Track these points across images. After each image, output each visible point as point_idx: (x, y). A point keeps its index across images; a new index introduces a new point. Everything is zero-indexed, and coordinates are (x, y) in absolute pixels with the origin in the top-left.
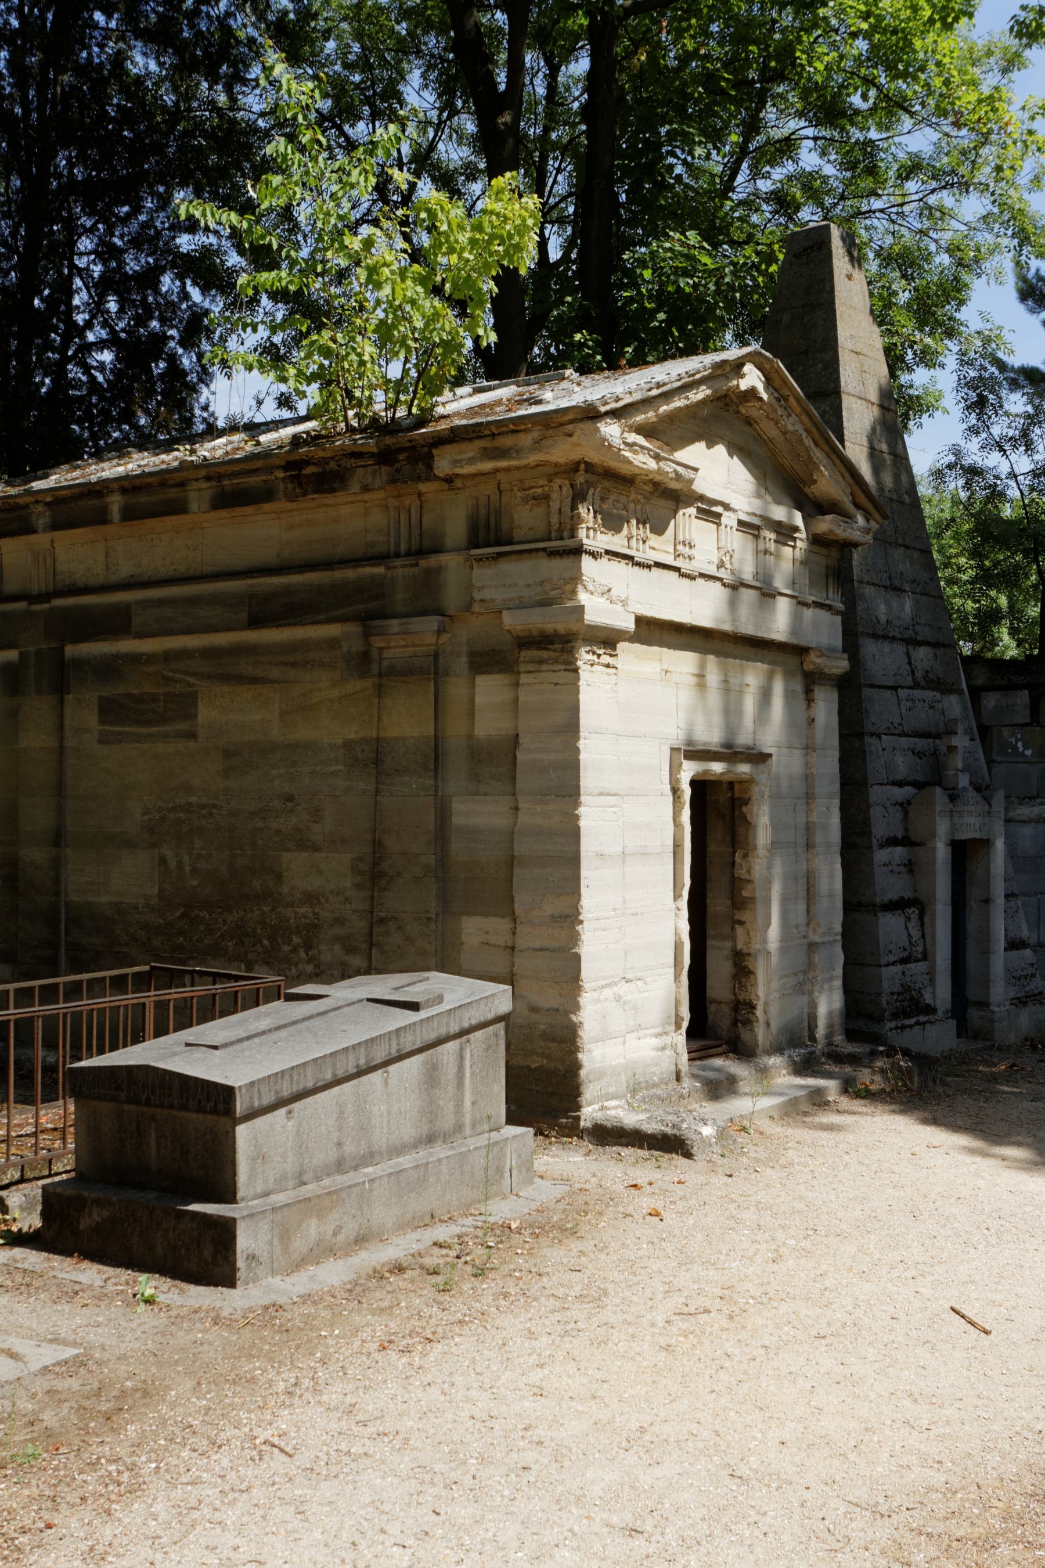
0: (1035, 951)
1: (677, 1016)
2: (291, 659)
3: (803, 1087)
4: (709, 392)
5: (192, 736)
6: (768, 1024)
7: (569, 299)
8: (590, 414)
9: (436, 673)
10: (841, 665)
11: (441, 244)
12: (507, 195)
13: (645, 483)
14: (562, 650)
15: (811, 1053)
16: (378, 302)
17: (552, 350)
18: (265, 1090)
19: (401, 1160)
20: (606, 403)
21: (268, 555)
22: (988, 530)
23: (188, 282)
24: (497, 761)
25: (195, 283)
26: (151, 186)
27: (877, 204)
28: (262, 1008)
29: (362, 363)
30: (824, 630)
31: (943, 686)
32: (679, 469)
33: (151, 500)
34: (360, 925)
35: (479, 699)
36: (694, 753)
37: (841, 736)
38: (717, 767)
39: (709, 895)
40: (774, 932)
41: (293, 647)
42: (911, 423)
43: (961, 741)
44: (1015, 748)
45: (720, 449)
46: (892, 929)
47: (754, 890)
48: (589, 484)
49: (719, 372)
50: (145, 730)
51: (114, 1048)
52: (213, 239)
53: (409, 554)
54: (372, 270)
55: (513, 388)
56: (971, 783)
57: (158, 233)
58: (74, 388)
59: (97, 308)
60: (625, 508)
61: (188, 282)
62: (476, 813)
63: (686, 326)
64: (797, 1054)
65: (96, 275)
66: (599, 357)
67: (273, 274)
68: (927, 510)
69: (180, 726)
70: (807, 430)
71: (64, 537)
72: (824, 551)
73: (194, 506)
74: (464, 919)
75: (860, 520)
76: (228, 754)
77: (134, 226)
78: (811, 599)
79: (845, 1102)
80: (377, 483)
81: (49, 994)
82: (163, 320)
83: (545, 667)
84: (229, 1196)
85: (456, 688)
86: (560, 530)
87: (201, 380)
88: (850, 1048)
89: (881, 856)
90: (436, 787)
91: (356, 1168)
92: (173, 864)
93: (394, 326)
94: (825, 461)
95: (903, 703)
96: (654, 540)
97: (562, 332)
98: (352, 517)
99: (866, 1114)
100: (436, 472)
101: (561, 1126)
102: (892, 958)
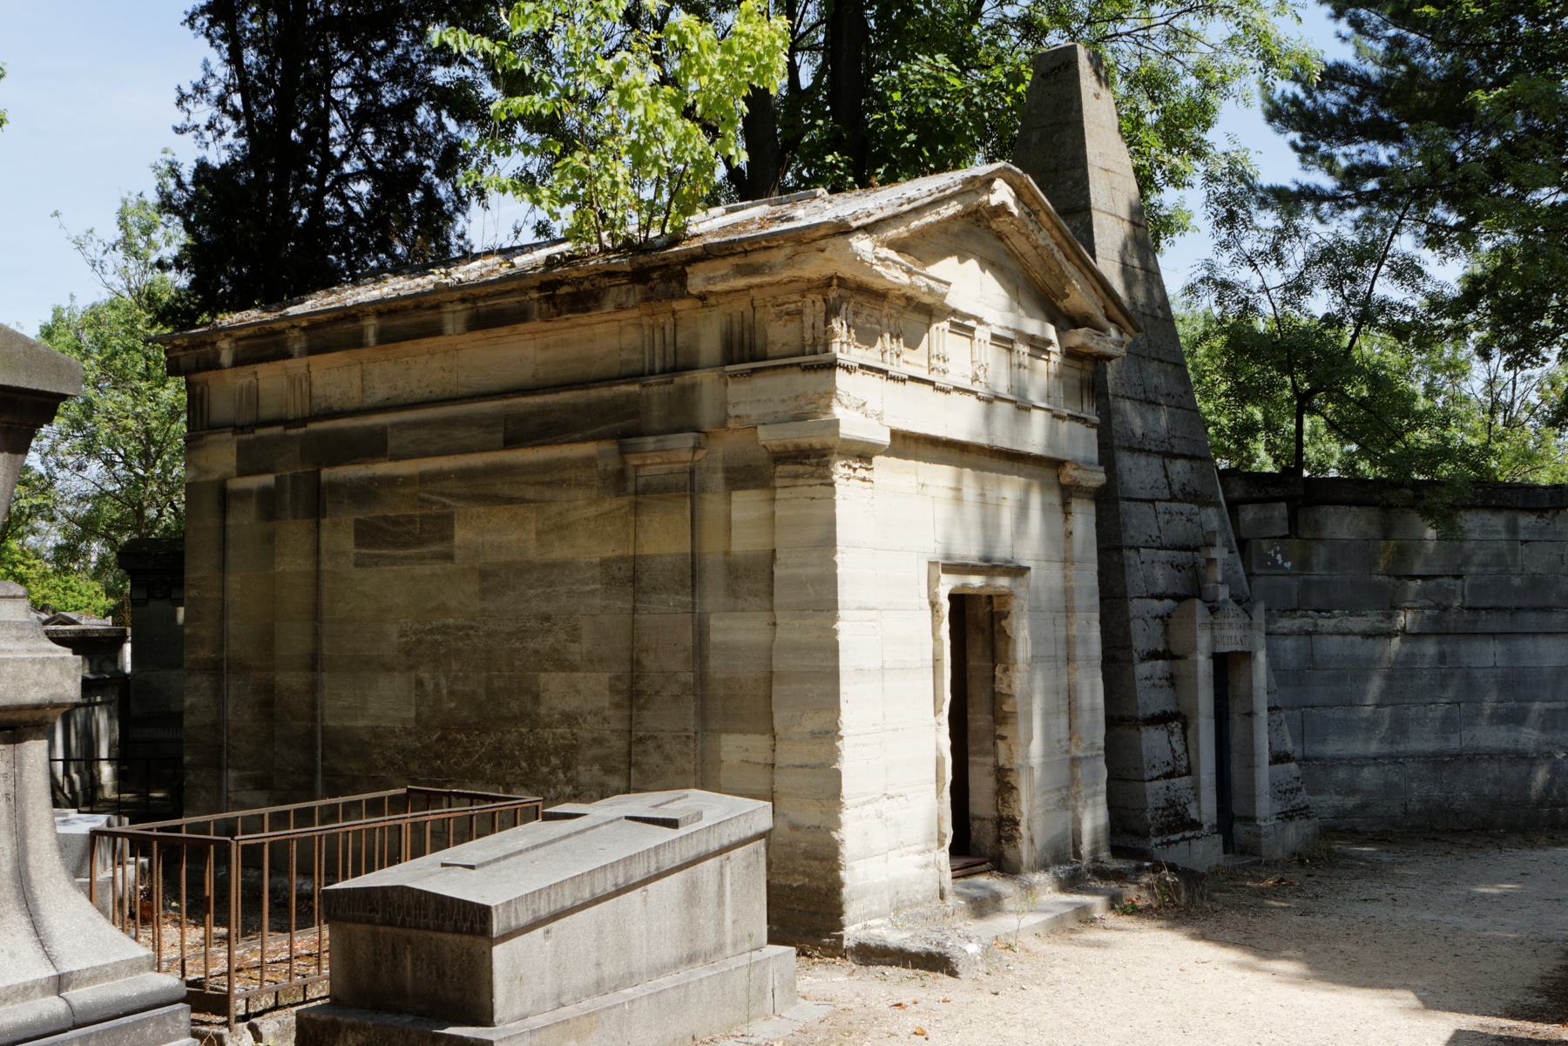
0: (1300, 766)
1: (940, 832)
2: (547, 479)
3: (1068, 904)
4: (960, 207)
5: (448, 557)
6: (1032, 841)
7: (820, 122)
8: (842, 230)
9: (692, 490)
10: (1098, 478)
11: (691, 67)
12: (755, 18)
13: (898, 297)
14: (818, 465)
15: (1076, 870)
16: (631, 123)
17: (805, 173)
18: (521, 908)
19: (661, 980)
20: (857, 219)
21: (522, 374)
22: (1241, 342)
23: (444, 113)
24: (756, 578)
25: (451, 115)
26: (406, 21)
27: (1122, 29)
28: (520, 828)
29: (615, 184)
30: (1080, 443)
31: (1200, 499)
32: (932, 283)
33: (407, 323)
34: (618, 744)
35: (735, 516)
36: (951, 568)
37: (1099, 550)
38: (976, 581)
39: (970, 710)
40: (1036, 748)
41: (548, 466)
42: (1163, 242)
43: (1219, 553)
44: (1274, 560)
45: (972, 264)
46: (1155, 743)
47: (1015, 704)
48: (841, 299)
49: (970, 187)
50: (402, 553)
51: (370, 869)
52: (468, 72)
53: (663, 371)
54: (624, 92)
55: (766, 207)
56: (1231, 596)
57: (414, 66)
58: (331, 218)
59: (354, 140)
60: (879, 323)
61: (444, 113)
62: (736, 630)
63: (936, 143)
64: (1063, 870)
65: (352, 108)
66: (850, 179)
67: (526, 98)
68: (1180, 328)
69: (436, 548)
70: (1058, 244)
71: (315, 359)
72: (1078, 365)
73: (449, 328)
74: (723, 736)
75: (1113, 333)
76: (484, 575)
77: (390, 60)
78: (1066, 412)
79: (1111, 919)
80: (631, 302)
81: (305, 817)
82: (419, 151)
83: (801, 481)
84: (486, 1019)
85: (712, 504)
86: (814, 345)
87: (457, 209)
88: (1116, 864)
89: (1142, 669)
90: (694, 604)
91: (615, 989)
92: (430, 686)
93: (646, 147)
94: (1078, 275)
95: (1161, 517)
96: (908, 354)
97: (814, 154)
98: (607, 335)
99: (1133, 931)
100: (690, 289)
101: (824, 947)
102: (1156, 773)
